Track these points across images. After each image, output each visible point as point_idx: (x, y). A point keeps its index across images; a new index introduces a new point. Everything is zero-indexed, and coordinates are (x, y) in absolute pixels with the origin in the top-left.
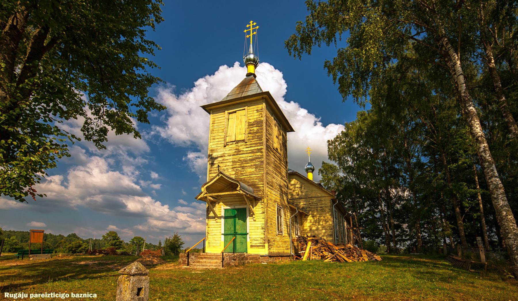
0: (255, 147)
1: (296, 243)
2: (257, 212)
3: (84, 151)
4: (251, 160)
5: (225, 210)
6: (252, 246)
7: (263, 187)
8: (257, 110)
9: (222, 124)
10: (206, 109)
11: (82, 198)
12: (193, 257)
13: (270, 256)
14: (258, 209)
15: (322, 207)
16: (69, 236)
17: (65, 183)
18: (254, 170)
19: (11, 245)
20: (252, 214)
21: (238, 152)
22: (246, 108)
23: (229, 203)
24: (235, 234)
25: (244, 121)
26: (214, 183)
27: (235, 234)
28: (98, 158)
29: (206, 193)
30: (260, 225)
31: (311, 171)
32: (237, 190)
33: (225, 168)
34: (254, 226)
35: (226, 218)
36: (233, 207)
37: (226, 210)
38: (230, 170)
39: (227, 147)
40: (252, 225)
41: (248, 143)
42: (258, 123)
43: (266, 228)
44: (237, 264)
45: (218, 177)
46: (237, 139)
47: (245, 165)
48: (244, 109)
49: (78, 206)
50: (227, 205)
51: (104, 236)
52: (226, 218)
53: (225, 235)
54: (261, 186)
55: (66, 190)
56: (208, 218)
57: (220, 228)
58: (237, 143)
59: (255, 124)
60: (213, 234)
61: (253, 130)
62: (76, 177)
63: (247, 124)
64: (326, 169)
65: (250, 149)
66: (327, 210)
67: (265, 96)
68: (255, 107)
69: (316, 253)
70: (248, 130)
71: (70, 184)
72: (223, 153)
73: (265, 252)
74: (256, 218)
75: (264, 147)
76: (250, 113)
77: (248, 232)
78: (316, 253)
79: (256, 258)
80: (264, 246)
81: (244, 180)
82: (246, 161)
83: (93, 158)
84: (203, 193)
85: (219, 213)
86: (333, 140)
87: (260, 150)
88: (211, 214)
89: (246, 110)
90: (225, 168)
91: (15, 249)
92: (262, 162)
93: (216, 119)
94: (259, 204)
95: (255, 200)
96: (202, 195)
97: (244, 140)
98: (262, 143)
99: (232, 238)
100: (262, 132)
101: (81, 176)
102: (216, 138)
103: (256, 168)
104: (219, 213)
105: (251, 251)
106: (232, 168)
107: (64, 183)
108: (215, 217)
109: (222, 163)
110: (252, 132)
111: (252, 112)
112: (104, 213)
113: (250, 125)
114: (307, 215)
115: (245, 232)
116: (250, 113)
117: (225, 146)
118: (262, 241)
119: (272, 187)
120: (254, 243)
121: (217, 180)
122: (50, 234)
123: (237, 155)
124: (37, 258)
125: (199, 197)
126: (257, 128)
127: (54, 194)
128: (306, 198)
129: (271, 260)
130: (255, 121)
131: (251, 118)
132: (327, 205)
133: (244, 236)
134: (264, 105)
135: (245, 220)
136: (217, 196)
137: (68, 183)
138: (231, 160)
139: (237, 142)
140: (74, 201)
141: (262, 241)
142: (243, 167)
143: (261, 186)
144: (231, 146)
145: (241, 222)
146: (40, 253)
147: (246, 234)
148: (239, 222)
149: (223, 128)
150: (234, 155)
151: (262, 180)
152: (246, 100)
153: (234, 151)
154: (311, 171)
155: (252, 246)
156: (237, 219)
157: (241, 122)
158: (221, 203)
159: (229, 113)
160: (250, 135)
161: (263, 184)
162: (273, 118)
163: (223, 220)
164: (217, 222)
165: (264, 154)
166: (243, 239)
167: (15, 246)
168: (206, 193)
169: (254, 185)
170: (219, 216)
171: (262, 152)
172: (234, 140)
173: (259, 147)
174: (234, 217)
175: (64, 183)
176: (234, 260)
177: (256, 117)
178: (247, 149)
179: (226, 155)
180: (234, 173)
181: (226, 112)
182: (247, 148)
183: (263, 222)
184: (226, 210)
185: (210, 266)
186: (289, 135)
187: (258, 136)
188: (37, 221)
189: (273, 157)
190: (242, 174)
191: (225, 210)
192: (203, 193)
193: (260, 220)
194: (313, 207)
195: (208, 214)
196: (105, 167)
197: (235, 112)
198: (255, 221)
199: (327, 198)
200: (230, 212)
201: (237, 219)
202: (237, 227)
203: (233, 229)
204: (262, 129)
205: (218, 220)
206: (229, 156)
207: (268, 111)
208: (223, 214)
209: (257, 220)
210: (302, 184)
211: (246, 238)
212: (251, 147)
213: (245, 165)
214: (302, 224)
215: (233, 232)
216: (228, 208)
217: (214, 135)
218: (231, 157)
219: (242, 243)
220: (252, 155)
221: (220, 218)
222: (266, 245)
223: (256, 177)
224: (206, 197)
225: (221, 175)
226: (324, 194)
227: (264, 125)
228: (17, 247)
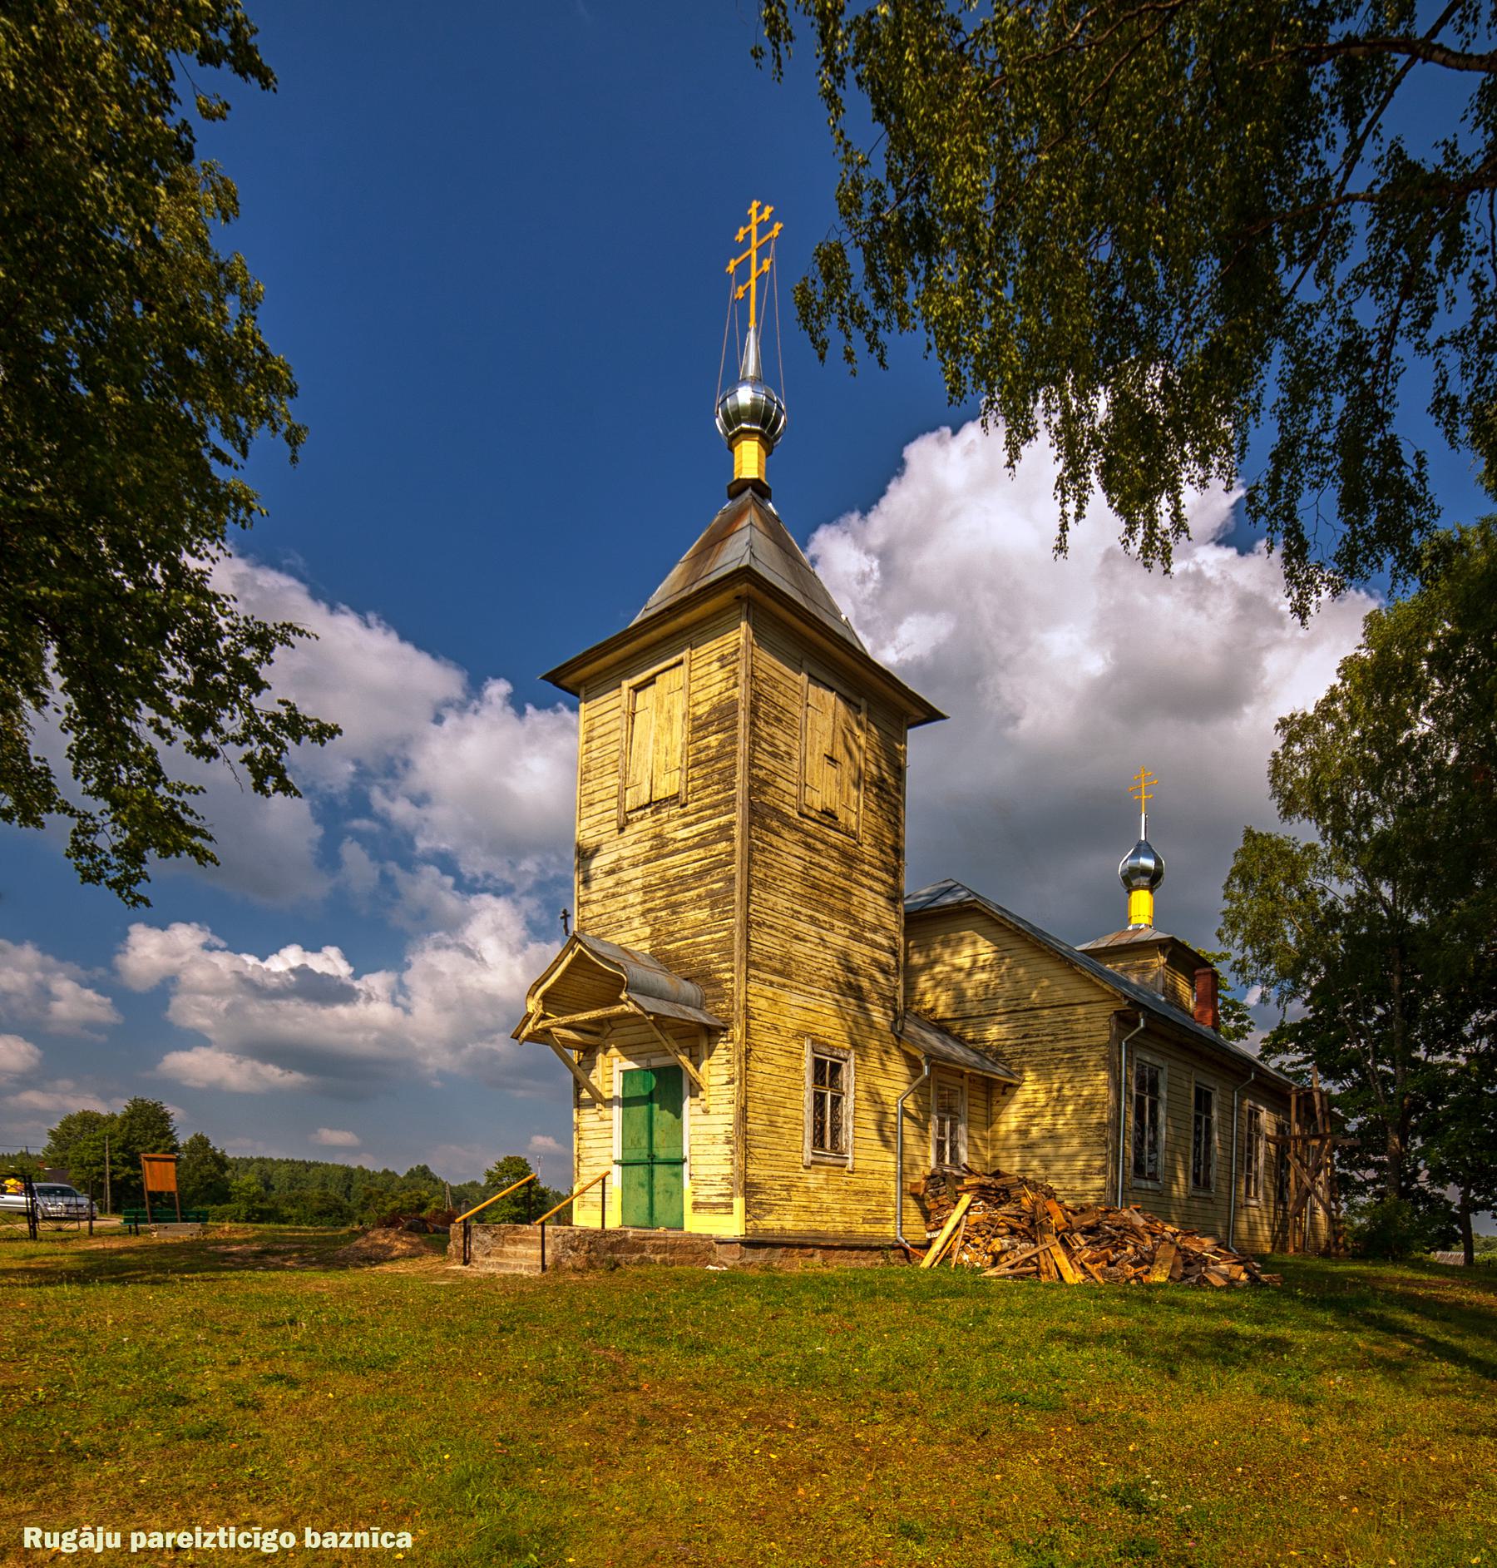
0: (711, 818)
1: (1028, 1198)
2: (713, 1081)
3: (449, 881)
4: (699, 875)
5: (625, 1073)
6: (696, 1206)
7: (732, 980)
8: (721, 658)
9: (613, 737)
10: (566, 682)
11: (455, 1046)
12: (487, 1237)
13: (751, 1243)
14: (715, 1072)
15: (1073, 1049)
16: (411, 1174)
17: (400, 999)
18: (703, 915)
19: (250, 1201)
20: (695, 1089)
21: (661, 846)
22: (684, 655)
23: (636, 1049)
24: (652, 1161)
25: (678, 712)
26: (558, 981)
27: (652, 1161)
28: (487, 898)
29: (543, 1017)
30: (721, 1129)
31: (1145, 881)
32: (623, 1003)
33: (623, 915)
34: (705, 1129)
35: (626, 1102)
36: (644, 1064)
37: (626, 1073)
38: (636, 923)
39: (628, 831)
40: (698, 1129)
41: (690, 807)
42: (723, 714)
43: (743, 1139)
44: (579, 1265)
45: (571, 956)
46: (659, 794)
47: (680, 897)
48: (680, 663)
49: (442, 1075)
50: (629, 1056)
51: (490, 1174)
52: (626, 1102)
53: (623, 1164)
54: (728, 976)
55: (410, 1018)
56: (580, 1104)
57: (608, 1142)
58: (657, 811)
59: (711, 723)
60: (593, 1161)
61: (708, 747)
62: (433, 975)
63: (688, 727)
64: (1261, 864)
65: (695, 829)
66: (1094, 1058)
67: (743, 588)
68: (712, 649)
69: (978, 1240)
70: (692, 749)
71: (415, 998)
72: (614, 856)
73: (732, 1225)
74: (711, 1100)
75: (738, 816)
76: (700, 673)
77: (686, 1154)
78: (978, 1240)
79: (703, 1248)
80: (731, 1206)
81: (677, 958)
82: (682, 882)
83: (475, 901)
84: (534, 1019)
85: (607, 1087)
86: (1311, 712)
87: (724, 832)
88: (585, 1095)
89: (685, 666)
90: (623, 915)
91: (261, 1211)
92: (731, 879)
93: (598, 722)
94: (721, 1051)
95: (701, 1037)
96: (530, 1024)
97: (676, 796)
98: (733, 799)
99: (640, 1172)
100: (734, 752)
101: (443, 968)
102: (597, 796)
103: (713, 906)
104: (607, 1087)
105: (697, 1224)
106: (643, 914)
107: (400, 995)
108: (597, 1100)
109: (614, 895)
110: (702, 756)
111: (705, 669)
112: (521, 1093)
113: (699, 727)
114: (1011, 1085)
115: (677, 1157)
116: (700, 673)
117: (621, 830)
118: (724, 1188)
119: (789, 977)
120: (707, 1193)
121: (570, 965)
122: (360, 1167)
123: (656, 859)
124: (168, 1233)
125: (524, 1034)
126: (721, 736)
127: (374, 1035)
128: (1018, 1011)
129: (752, 1257)
130: (714, 709)
131: (700, 697)
132: (1094, 1041)
133: (676, 1169)
134: (741, 633)
135: (678, 1113)
136: (598, 1022)
137: (409, 998)
138: (638, 883)
139: (656, 805)
140: (430, 1061)
141: (724, 1188)
142: (674, 908)
143: (728, 976)
144: (638, 826)
145: (667, 1116)
146: (176, 1221)
147: (681, 1162)
148: (663, 1117)
149: (615, 756)
150: (648, 861)
151: (728, 954)
152: (682, 620)
153: (648, 844)
154: (1145, 881)
155: (696, 1206)
156: (656, 1106)
157: (670, 719)
158: (614, 1051)
159: (637, 689)
160: (696, 772)
161: (732, 970)
162: (803, 678)
163: (617, 1111)
164: (602, 1120)
165: (738, 844)
166: (673, 1179)
167: (257, 1205)
168: (543, 1017)
169: (703, 976)
170: (607, 1096)
171: (731, 839)
172: (646, 801)
173: (723, 820)
174: (649, 1099)
175: (400, 995)
176: (572, 1248)
177: (715, 690)
178: (684, 833)
179: (625, 864)
180: (648, 930)
181: (626, 684)
182: (687, 825)
183: (731, 1118)
184: (626, 1073)
185: (515, 1267)
186: (919, 744)
187: (721, 772)
188: (333, 1127)
189: (799, 851)
190: (671, 934)
191: (625, 1073)
192: (534, 1019)
193: (722, 1109)
194: (1037, 1047)
195: (578, 1091)
196: (516, 931)
197: (651, 681)
198: (706, 1112)
199: (1096, 1008)
200: (638, 1079)
201: (656, 1106)
202: (658, 1137)
203: (644, 1142)
204: (733, 740)
205: (606, 1113)
206: (635, 866)
207: (773, 650)
208: (617, 1091)
209: (712, 1109)
210: (1002, 952)
211: (679, 1176)
212: (698, 821)
213: (680, 897)
214: (990, 1121)
215: (644, 1157)
216: (632, 1065)
217: (591, 787)
218: (638, 872)
219: (670, 1194)
220: (701, 852)
221: (609, 1103)
222: (739, 1203)
223: (713, 941)
224: (547, 1031)
225: (579, 947)
226: (1085, 994)
227: (742, 718)
228: (265, 1206)
